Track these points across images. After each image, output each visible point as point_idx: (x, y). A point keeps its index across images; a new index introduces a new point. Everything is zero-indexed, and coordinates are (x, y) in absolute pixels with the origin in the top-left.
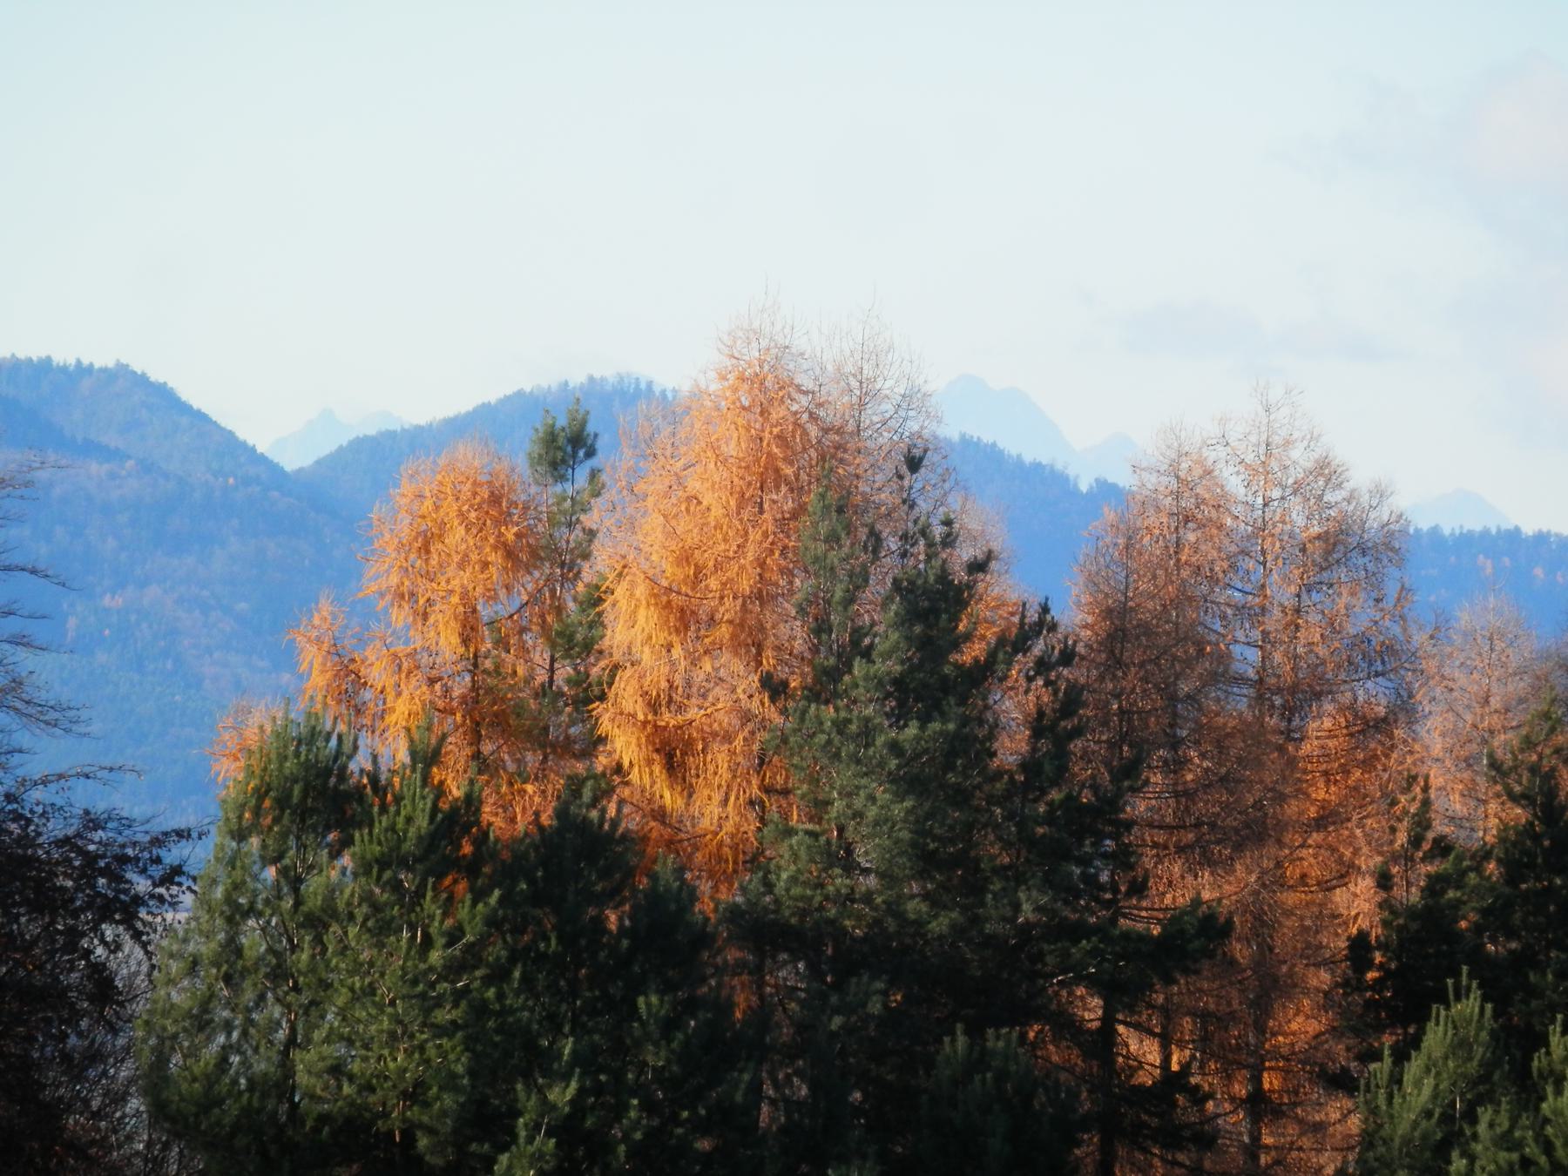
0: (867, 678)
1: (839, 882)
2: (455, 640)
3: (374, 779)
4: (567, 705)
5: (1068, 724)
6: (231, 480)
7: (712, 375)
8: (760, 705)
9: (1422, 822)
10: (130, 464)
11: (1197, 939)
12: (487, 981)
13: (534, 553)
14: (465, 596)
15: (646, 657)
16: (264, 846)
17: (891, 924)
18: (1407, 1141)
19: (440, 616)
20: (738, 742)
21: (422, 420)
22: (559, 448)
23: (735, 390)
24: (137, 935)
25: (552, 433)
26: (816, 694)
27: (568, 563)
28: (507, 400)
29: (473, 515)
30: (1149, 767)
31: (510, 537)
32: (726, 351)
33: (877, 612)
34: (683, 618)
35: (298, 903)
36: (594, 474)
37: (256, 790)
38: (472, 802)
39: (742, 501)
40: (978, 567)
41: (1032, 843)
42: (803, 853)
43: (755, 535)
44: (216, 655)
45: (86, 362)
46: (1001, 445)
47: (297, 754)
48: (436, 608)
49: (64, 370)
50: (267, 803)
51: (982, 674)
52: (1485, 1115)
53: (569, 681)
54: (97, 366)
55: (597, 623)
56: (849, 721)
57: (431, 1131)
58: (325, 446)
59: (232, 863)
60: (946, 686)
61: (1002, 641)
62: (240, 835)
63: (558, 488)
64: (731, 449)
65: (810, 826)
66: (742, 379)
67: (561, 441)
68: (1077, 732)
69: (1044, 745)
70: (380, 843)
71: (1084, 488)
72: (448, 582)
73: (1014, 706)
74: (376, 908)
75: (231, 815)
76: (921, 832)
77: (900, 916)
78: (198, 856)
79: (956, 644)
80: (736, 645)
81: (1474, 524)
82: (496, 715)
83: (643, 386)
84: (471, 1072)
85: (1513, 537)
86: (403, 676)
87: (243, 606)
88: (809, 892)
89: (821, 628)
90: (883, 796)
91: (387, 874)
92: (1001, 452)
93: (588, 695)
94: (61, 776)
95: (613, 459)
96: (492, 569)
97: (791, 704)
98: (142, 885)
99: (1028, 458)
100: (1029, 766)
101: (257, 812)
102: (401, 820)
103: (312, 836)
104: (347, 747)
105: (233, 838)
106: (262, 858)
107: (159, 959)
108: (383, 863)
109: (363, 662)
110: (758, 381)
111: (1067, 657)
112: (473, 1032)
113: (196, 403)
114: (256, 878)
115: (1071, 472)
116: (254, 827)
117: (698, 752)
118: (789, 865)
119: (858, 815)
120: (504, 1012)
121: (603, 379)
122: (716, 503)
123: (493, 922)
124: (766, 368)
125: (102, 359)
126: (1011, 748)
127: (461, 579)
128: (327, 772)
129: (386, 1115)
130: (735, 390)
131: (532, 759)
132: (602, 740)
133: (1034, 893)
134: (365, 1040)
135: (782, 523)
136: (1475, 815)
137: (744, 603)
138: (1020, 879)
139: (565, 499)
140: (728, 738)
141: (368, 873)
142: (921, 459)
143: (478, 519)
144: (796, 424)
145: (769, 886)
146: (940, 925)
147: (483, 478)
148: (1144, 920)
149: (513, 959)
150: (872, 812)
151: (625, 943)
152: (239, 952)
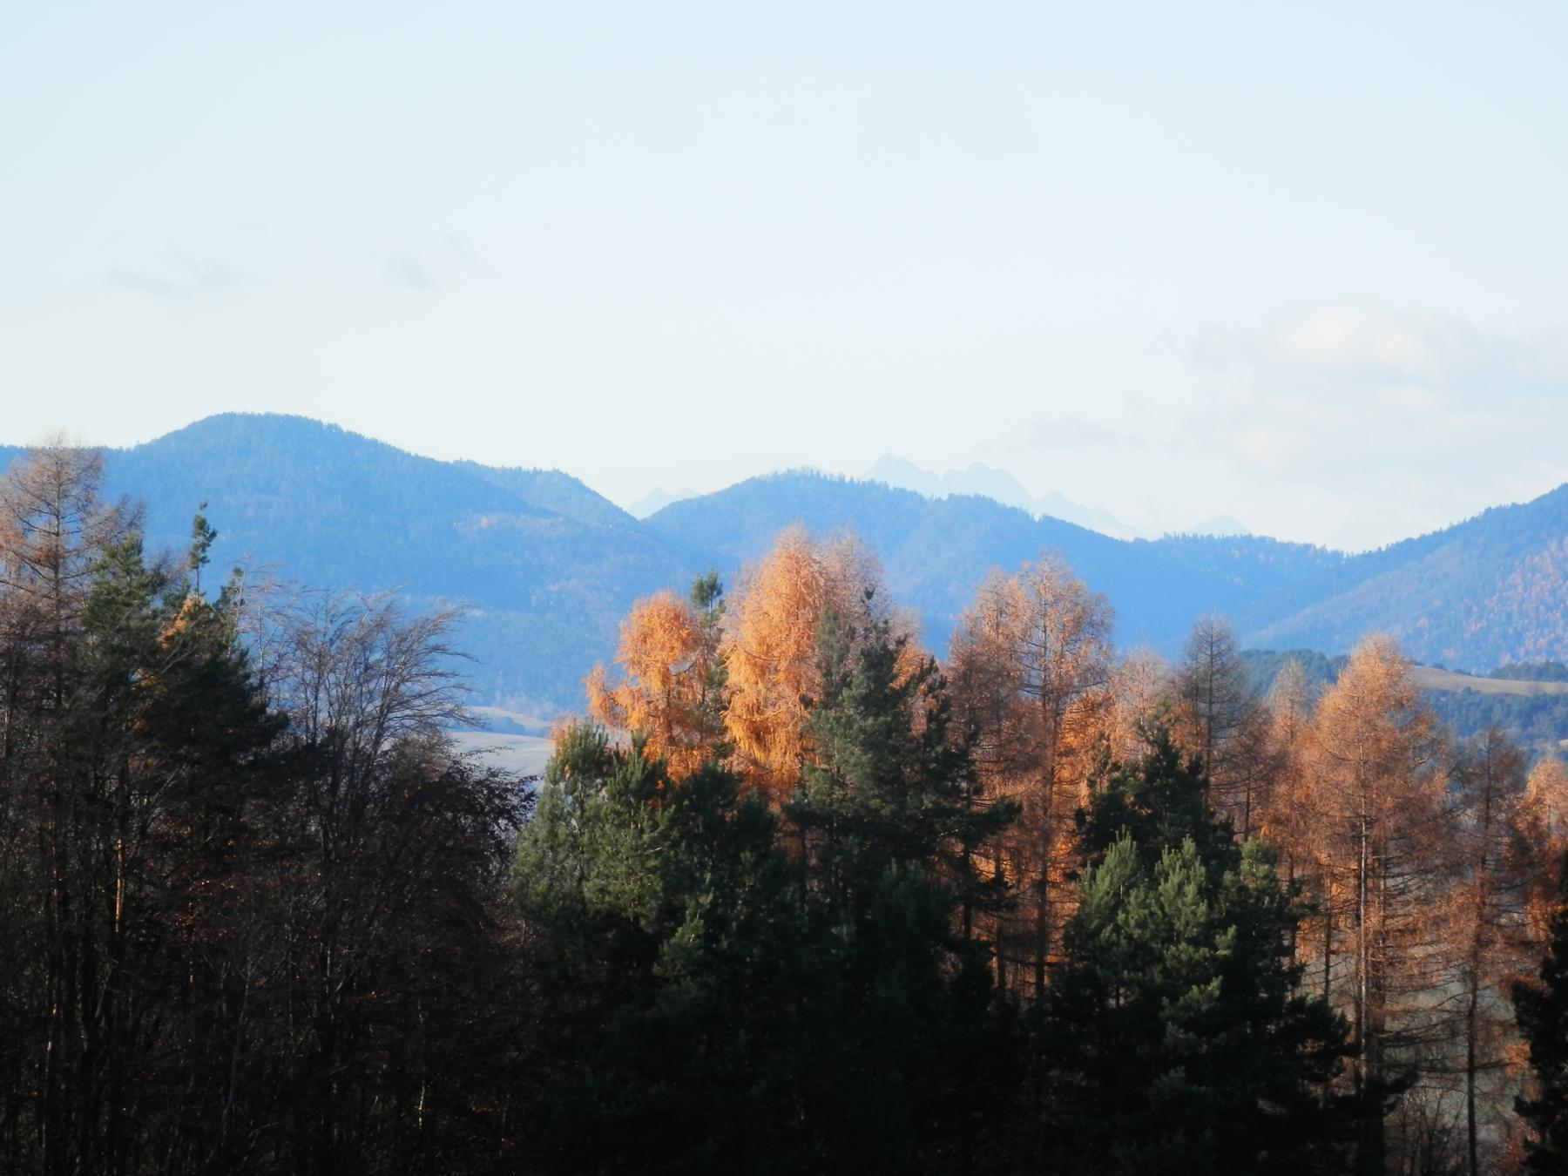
3: (617, 754)
5: (944, 716)
8: (799, 710)
11: (1008, 812)
13: (695, 641)
17: (863, 812)
18: (1098, 906)
20: (790, 728)
24: (515, 825)
26: (826, 706)
33: (854, 666)
34: (763, 669)
36: (721, 602)
39: (789, 614)
40: (901, 643)
41: (928, 771)
49: (528, 473)
51: (904, 693)
52: (1133, 893)
55: (724, 672)
57: (646, 917)
58: (657, 507)
60: (886, 698)
61: (913, 677)
68: (949, 719)
69: (933, 726)
73: (920, 705)
74: (618, 814)
76: (876, 768)
77: (867, 807)
78: (539, 787)
79: (895, 677)
81: (1230, 533)
84: (665, 890)
85: (1248, 539)
87: (617, 589)
89: (828, 674)
90: (857, 751)
93: (722, 706)
95: (730, 596)
99: (1009, 505)
100: (927, 736)
101: (563, 771)
107: (523, 839)
111: (943, 685)
112: (664, 871)
113: (593, 487)
117: (772, 734)
118: (815, 785)
119: (846, 761)
120: (679, 862)
122: (776, 615)
125: (546, 467)
126: (919, 726)
127: (661, 656)
129: (625, 910)
131: (696, 737)
132: (726, 728)
134: (618, 875)
135: (809, 624)
136: (1132, 749)
138: (923, 790)
145: (805, 795)
146: (885, 812)
148: (984, 803)
149: (682, 837)
150: (853, 760)
152: (556, 836)
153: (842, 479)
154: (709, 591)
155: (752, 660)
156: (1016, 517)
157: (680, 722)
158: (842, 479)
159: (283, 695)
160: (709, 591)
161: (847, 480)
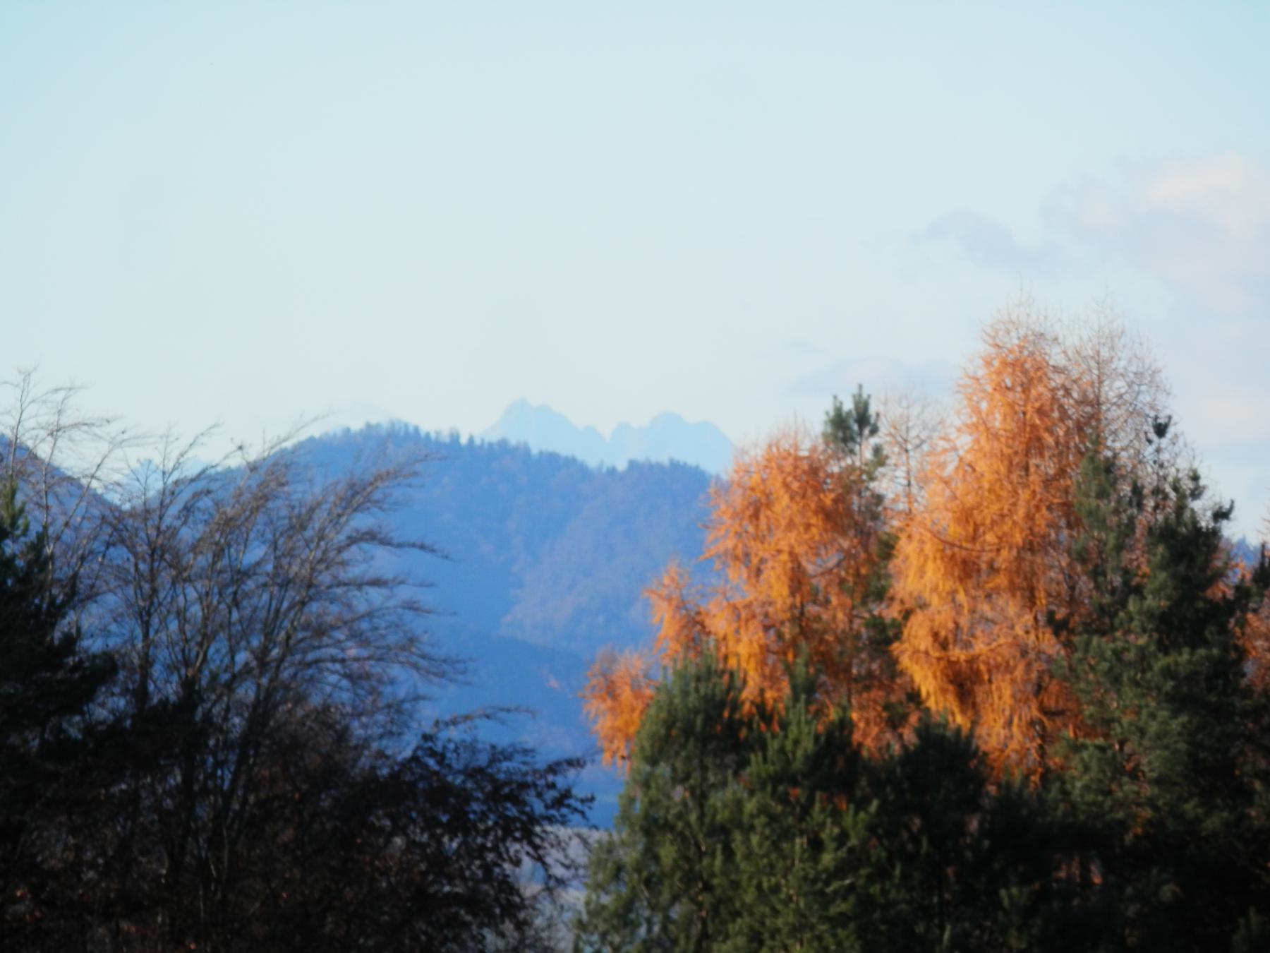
0: (1140, 612)
7: (980, 362)
12: (870, 879)
15: (935, 601)
19: (772, 573)
20: (1019, 672)
23: (999, 373)
32: (991, 341)
33: (1143, 560)
34: (965, 568)
35: (701, 817)
37: (665, 722)
40: (1222, 515)
42: (1094, 765)
43: (1024, 495)
47: (697, 690)
59: (646, 784)
62: (653, 761)
64: (997, 422)
66: (1005, 364)
70: (773, 764)
74: (773, 819)
80: (1013, 589)
88: (1100, 798)
90: (1163, 714)
91: (781, 788)
93: (884, 637)
94: (467, 718)
97: (1076, 639)
98: (539, 808)
102: (789, 745)
104: (738, 683)
108: (776, 780)
110: (1016, 365)
114: (669, 797)
119: (1142, 732)
121: (378, 425)
123: (872, 828)
124: (1026, 353)
127: (788, 540)
128: (722, 704)
130: (999, 373)
137: (1019, 553)
140: (1009, 669)
141: (763, 788)
146: (8, 917)
150: (1153, 727)
151: (986, 843)
153: (455, 438)
158: (455, 438)
159: (99, 625)
161: (464, 440)
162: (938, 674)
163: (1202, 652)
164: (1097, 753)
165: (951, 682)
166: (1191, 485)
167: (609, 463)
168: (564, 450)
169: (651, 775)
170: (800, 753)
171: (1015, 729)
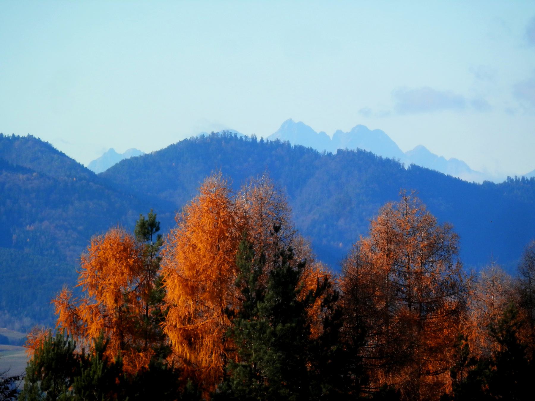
0: (262, 308)
1: (256, 383)
2: (113, 302)
4: (153, 322)
6: (75, 179)
8: (225, 320)
9: (467, 352)
10: (35, 174)
14: (115, 285)
16: (42, 384)
20: (216, 333)
21: (148, 151)
22: (146, 228)
25: (143, 223)
27: (153, 268)
28: (180, 143)
29: (118, 255)
30: (368, 336)
31: (131, 263)
34: (192, 289)
37: (39, 364)
38: (119, 364)
40: (302, 265)
44: (71, 247)
45: (16, 135)
46: (373, 153)
47: (53, 350)
48: (105, 290)
49: (8, 138)
50: (43, 369)
53: (153, 313)
54: (21, 136)
56: (256, 324)
62: (34, 381)
63: (146, 243)
65: (244, 363)
67: (147, 226)
70: (84, 381)
71: (406, 168)
72: (109, 280)
75: (30, 374)
82: (128, 328)
83: (233, 135)
86: (94, 315)
87: (80, 228)
88: (244, 388)
89: (246, 291)
90: (270, 351)
92: (373, 155)
93: (161, 317)
96: (125, 275)
99: (384, 157)
102: (92, 372)
103: (60, 380)
104: (72, 347)
105: (31, 382)
106: (42, 389)
109: (79, 310)
113: (60, 149)
115: (401, 162)
116: (39, 377)
119: (261, 359)
121: (218, 133)
125: (22, 133)
126: (317, 331)
133: (327, 385)
139: (149, 247)
142: (279, 227)
143: (119, 257)
144: (230, 216)
145: (230, 387)
147: (121, 242)
150: (266, 357)
154: (149, 228)
155: (184, 281)
156: (390, 167)
157: (130, 331)
160: (149, 228)
161: (259, 140)
162: (180, 335)
163: (288, 325)
164: (243, 369)
165: (185, 339)
166: (288, 253)
167: (328, 151)
168: (307, 145)
169: (32, 387)
170: (96, 377)
171: (213, 358)
